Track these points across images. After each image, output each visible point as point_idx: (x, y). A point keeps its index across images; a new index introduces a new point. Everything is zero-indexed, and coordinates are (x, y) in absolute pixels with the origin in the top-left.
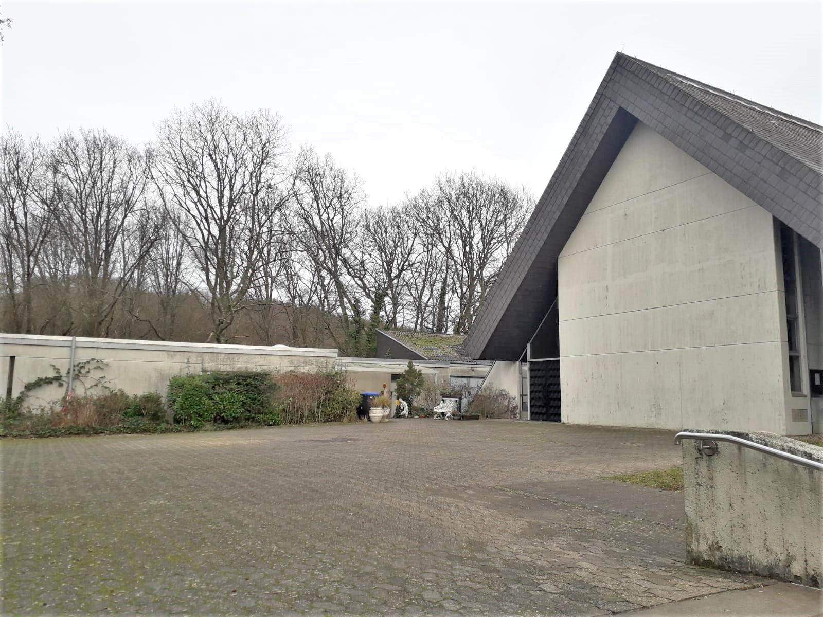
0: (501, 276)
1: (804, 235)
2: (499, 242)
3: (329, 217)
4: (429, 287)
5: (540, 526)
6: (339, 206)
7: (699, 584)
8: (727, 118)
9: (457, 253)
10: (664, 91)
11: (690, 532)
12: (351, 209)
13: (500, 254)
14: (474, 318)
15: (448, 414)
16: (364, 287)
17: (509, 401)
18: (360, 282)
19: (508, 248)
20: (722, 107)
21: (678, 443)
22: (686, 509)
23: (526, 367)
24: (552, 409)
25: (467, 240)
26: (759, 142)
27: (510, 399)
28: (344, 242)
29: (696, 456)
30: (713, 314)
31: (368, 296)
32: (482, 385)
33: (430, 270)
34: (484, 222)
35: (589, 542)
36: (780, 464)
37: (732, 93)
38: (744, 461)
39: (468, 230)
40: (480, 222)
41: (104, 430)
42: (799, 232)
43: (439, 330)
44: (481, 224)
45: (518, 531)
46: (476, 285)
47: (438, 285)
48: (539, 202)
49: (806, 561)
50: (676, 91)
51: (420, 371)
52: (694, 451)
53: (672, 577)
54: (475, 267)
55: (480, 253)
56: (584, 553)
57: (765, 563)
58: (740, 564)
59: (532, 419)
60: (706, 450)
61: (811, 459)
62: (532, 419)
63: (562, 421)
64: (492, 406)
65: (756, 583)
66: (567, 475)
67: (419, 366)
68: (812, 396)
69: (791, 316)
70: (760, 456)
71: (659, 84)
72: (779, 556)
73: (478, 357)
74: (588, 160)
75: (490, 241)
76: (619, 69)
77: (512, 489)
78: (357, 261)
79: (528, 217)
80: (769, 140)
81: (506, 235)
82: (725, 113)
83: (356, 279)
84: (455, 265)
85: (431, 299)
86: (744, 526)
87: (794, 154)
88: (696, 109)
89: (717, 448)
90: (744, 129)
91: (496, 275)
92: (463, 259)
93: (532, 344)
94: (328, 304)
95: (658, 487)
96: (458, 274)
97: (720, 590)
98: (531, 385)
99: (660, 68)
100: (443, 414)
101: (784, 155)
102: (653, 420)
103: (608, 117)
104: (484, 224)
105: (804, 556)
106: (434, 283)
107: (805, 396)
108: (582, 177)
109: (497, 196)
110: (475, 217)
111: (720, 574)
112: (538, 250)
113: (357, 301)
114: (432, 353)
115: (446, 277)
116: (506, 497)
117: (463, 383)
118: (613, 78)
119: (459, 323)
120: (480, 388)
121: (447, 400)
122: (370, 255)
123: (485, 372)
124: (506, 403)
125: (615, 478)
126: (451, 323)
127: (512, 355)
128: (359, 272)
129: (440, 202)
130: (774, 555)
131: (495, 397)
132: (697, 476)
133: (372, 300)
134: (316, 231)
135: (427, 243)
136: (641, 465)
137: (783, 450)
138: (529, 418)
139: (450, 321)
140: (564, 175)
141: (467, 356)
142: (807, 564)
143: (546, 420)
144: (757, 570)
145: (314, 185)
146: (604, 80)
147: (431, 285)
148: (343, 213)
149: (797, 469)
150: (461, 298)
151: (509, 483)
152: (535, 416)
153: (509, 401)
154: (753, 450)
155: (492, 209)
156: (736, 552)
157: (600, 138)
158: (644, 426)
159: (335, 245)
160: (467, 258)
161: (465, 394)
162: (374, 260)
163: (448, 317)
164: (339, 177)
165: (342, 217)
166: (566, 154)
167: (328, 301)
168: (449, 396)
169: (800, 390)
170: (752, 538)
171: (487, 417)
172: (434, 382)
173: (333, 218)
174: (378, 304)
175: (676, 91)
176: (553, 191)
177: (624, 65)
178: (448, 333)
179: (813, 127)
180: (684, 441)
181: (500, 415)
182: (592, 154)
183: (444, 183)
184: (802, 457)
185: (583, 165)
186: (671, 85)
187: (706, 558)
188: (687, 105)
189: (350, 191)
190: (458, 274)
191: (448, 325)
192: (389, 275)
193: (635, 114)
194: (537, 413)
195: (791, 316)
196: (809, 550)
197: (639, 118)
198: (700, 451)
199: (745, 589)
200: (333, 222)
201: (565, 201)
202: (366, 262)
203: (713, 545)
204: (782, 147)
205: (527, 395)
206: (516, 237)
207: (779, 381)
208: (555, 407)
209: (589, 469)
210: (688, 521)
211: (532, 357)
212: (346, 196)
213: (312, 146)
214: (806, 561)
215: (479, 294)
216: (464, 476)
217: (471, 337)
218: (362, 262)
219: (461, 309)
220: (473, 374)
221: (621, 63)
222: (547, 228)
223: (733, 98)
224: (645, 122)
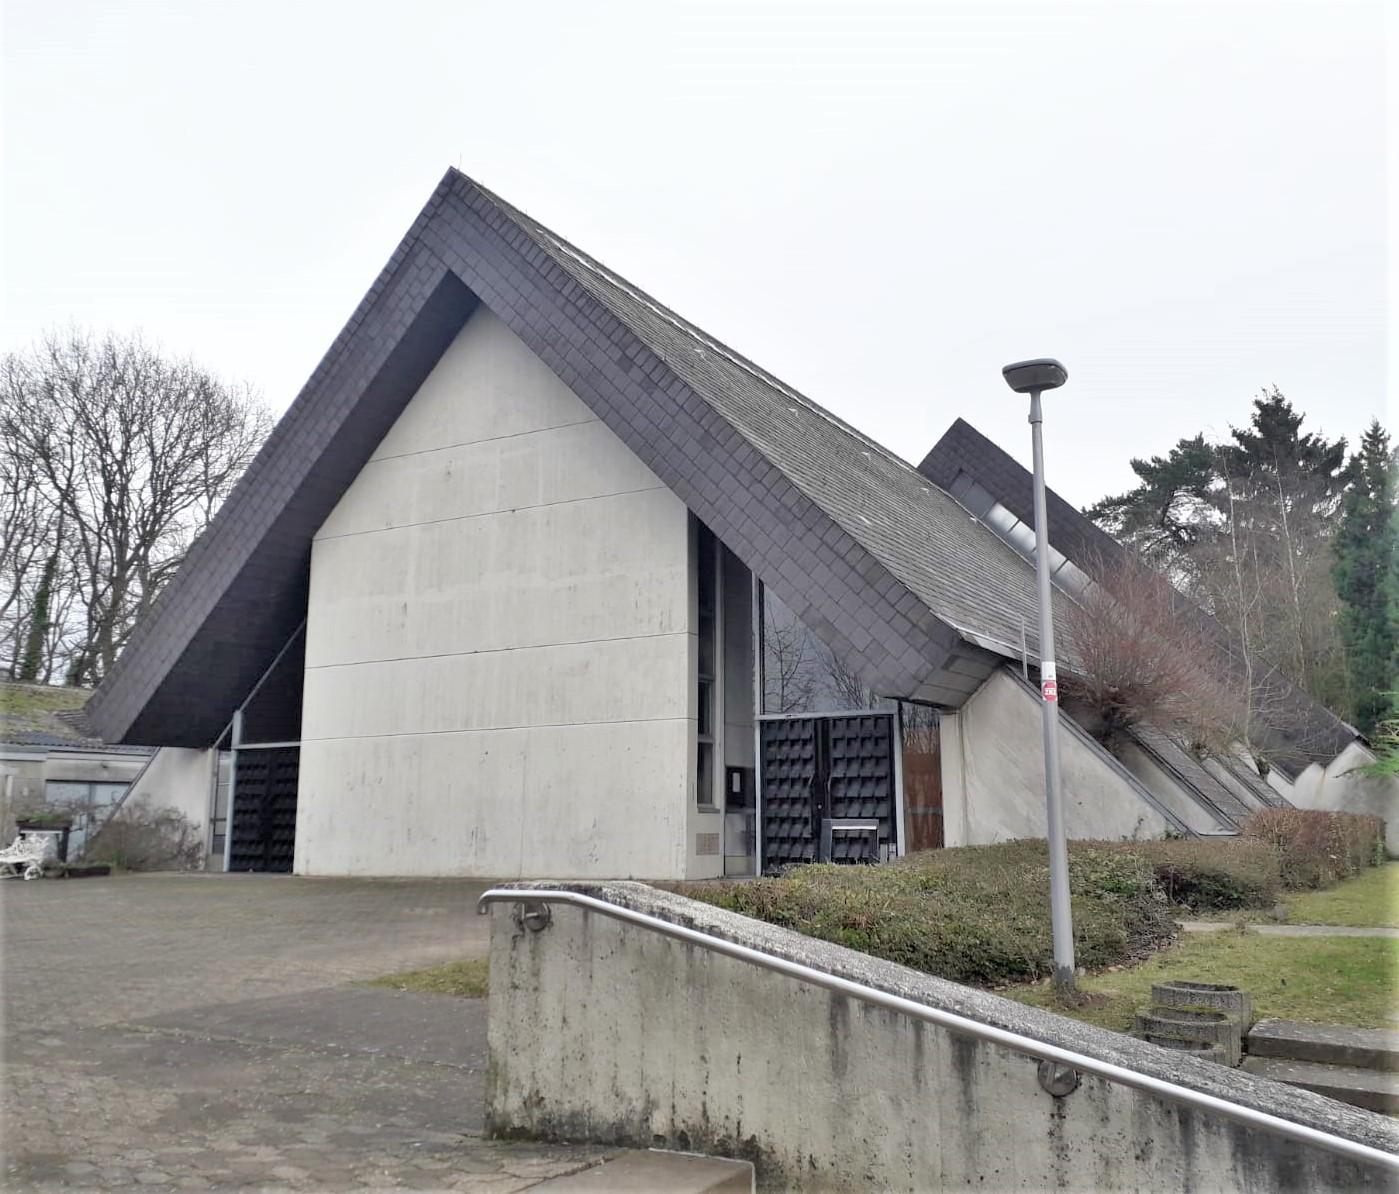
0: (189, 566)
1: (731, 546)
2: (190, 492)
4: (12, 575)
5: (204, 1100)
7: (496, 1177)
8: (628, 330)
9: (91, 504)
10: (529, 258)
11: (493, 1077)
13: (191, 518)
14: (119, 651)
15: (32, 867)
17: (184, 833)
19: (209, 507)
20: (623, 311)
21: (484, 911)
22: (490, 1034)
23: (229, 761)
24: (277, 848)
25: (115, 481)
26: (673, 381)
27: (186, 827)
29: (513, 934)
30: (587, 666)
32: (124, 799)
33: (18, 536)
34: (158, 444)
35: (303, 1120)
36: (646, 938)
37: (640, 288)
38: (591, 938)
39: (119, 457)
40: (151, 445)
41: (476, 837)
42: (722, 539)
43: (29, 673)
44: (152, 452)
45: (152, 1118)
46: (131, 578)
47: (35, 573)
48: (282, 423)
49: (673, 1107)
50: (549, 264)
52: (511, 925)
53: (450, 1171)
54: (131, 540)
55: (144, 511)
56: (287, 1147)
57: (611, 1117)
58: (573, 1126)
59: (232, 869)
60: (532, 921)
61: (691, 928)
62: (232, 869)
63: (295, 871)
64: (143, 845)
65: (592, 1159)
66: (283, 984)
68: (727, 812)
69: (705, 676)
70: (617, 925)
71: (521, 245)
72: (634, 1103)
73: (119, 737)
74: (382, 358)
75: (170, 489)
76: (452, 199)
77: (157, 1027)
79: (257, 448)
80: (689, 380)
81: (206, 481)
82: (625, 319)
84: (83, 530)
85: (15, 603)
86: (583, 1055)
87: (722, 410)
88: (580, 303)
89: (549, 916)
90: (653, 355)
91: (179, 561)
92: (101, 520)
93: (245, 713)
95: (458, 993)
96: (88, 552)
97: (530, 1182)
98: (237, 798)
99: (525, 216)
100: (20, 867)
101: (709, 411)
102: (470, 861)
103: (423, 286)
104: (159, 451)
105: (671, 1100)
106: (25, 567)
107: (718, 811)
108: (370, 389)
109: (191, 396)
110: (136, 434)
111: (537, 1150)
115: (55, 556)
116: (138, 1046)
117: (76, 796)
118: (439, 212)
119: (81, 661)
120: (119, 806)
121: (33, 836)
123: (133, 770)
124: (177, 837)
125: (380, 982)
126: (60, 659)
127: (199, 736)
129: (50, 389)
130: (626, 1103)
131: (153, 826)
132: (512, 971)
135: (13, 474)
136: (435, 951)
137: (652, 913)
138: (226, 866)
139: (62, 655)
140: (333, 378)
141: (94, 735)
142: (674, 1112)
143: (263, 870)
144: (598, 1133)
146: (423, 214)
147: (16, 571)
149: (669, 945)
150: (91, 606)
151: (151, 1012)
152: (240, 862)
153: (184, 833)
154: (604, 917)
155: (177, 422)
156: (567, 1106)
157: (409, 319)
158: (454, 873)
160: (114, 516)
161: (81, 819)
163: (55, 645)
166: (341, 338)
168: (38, 826)
169: (711, 801)
170: (593, 1077)
171: (129, 868)
172: (4, 794)
175: (549, 264)
176: (310, 406)
177: (462, 194)
178: (51, 682)
179: (756, 371)
180: (495, 906)
181: (162, 863)
182: (392, 348)
183: (65, 348)
184: (679, 924)
185: (374, 363)
186: (541, 250)
187: (517, 1123)
188: (566, 292)
190: (88, 552)
191: (54, 666)
193: (476, 288)
194: (243, 857)
195: (705, 676)
196: (679, 1087)
197: (482, 298)
198: (521, 923)
199: (574, 1172)
201: (333, 431)
203: (530, 1097)
204: (707, 397)
205: (225, 820)
206: (229, 484)
207: (681, 785)
208: (284, 843)
209: (332, 967)
210: (490, 1057)
211: (244, 740)
214: (673, 1107)
215: (137, 600)
216: (43, 1007)
217: (106, 693)
219: (90, 628)
220: (105, 776)
222: (292, 477)
223: (640, 297)
224: (491, 307)
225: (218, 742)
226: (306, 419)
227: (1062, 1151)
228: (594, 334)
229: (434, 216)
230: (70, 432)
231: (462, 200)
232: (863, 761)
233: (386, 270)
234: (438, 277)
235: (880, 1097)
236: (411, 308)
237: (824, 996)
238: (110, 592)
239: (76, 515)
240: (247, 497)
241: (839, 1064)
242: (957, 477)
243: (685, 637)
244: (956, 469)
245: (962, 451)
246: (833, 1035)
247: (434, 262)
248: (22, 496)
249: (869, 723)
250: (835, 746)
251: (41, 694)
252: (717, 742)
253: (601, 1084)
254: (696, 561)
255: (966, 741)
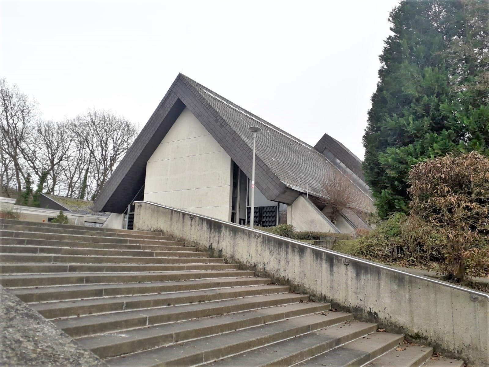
3: (13, 122)
4: (79, 173)
6: (21, 116)
9: (98, 154)
12: (30, 119)
13: (121, 157)
16: (34, 168)
18: (32, 165)
28: (22, 138)
31: (37, 173)
47: (84, 171)
51: (66, 216)
67: (65, 214)
78: (31, 151)
83: (29, 162)
88: (207, 106)
92: (100, 158)
94: (7, 176)
108: (160, 126)
112: (137, 157)
113: (29, 175)
114: (75, 209)
122: (40, 148)
123: (104, 220)
128: (31, 159)
133: (39, 175)
134: (4, 129)
135: (79, 146)
145: (4, 101)
148: (24, 121)
157: (169, 110)
159: (16, 140)
160: (104, 158)
162: (42, 152)
164: (22, 98)
165: (23, 123)
166: (154, 114)
167: (7, 173)
173: (17, 123)
174: (43, 179)
176: (146, 130)
186: (199, 93)
189: (30, 108)
192: (52, 161)
193: (184, 102)
200: (17, 126)
202: (37, 153)
211: (130, 212)
212: (27, 111)
213: (5, 78)
218: (34, 152)
220: (98, 221)
221: (181, 79)
225: (125, 212)
226: (145, 133)
227: (191, 226)
228: (210, 113)
229: (176, 84)
230: (93, 135)
231: (182, 81)
232: (270, 217)
233: (164, 98)
234: (176, 99)
235: (175, 222)
236: (169, 107)
237: (171, 210)
238: (102, 177)
239: (95, 157)
240: (131, 152)
241: (171, 219)
242: (325, 149)
243: (229, 187)
244: (324, 147)
245: (326, 142)
246: (171, 216)
247: (175, 96)
248: (81, 152)
249: (272, 208)
250: (264, 213)
251: (84, 202)
252: (237, 212)
253: (146, 226)
254: (233, 167)
255: (292, 212)
